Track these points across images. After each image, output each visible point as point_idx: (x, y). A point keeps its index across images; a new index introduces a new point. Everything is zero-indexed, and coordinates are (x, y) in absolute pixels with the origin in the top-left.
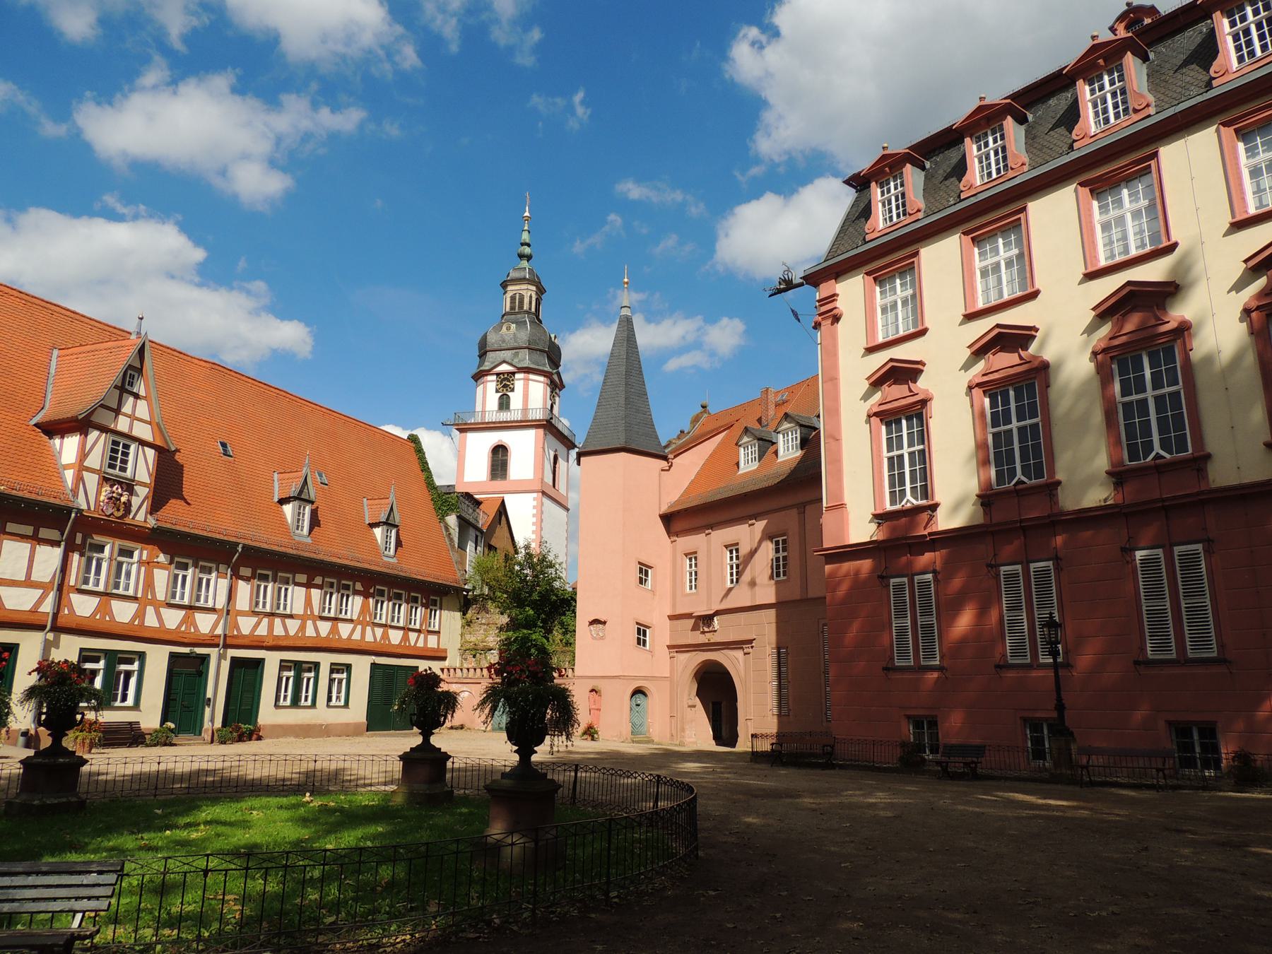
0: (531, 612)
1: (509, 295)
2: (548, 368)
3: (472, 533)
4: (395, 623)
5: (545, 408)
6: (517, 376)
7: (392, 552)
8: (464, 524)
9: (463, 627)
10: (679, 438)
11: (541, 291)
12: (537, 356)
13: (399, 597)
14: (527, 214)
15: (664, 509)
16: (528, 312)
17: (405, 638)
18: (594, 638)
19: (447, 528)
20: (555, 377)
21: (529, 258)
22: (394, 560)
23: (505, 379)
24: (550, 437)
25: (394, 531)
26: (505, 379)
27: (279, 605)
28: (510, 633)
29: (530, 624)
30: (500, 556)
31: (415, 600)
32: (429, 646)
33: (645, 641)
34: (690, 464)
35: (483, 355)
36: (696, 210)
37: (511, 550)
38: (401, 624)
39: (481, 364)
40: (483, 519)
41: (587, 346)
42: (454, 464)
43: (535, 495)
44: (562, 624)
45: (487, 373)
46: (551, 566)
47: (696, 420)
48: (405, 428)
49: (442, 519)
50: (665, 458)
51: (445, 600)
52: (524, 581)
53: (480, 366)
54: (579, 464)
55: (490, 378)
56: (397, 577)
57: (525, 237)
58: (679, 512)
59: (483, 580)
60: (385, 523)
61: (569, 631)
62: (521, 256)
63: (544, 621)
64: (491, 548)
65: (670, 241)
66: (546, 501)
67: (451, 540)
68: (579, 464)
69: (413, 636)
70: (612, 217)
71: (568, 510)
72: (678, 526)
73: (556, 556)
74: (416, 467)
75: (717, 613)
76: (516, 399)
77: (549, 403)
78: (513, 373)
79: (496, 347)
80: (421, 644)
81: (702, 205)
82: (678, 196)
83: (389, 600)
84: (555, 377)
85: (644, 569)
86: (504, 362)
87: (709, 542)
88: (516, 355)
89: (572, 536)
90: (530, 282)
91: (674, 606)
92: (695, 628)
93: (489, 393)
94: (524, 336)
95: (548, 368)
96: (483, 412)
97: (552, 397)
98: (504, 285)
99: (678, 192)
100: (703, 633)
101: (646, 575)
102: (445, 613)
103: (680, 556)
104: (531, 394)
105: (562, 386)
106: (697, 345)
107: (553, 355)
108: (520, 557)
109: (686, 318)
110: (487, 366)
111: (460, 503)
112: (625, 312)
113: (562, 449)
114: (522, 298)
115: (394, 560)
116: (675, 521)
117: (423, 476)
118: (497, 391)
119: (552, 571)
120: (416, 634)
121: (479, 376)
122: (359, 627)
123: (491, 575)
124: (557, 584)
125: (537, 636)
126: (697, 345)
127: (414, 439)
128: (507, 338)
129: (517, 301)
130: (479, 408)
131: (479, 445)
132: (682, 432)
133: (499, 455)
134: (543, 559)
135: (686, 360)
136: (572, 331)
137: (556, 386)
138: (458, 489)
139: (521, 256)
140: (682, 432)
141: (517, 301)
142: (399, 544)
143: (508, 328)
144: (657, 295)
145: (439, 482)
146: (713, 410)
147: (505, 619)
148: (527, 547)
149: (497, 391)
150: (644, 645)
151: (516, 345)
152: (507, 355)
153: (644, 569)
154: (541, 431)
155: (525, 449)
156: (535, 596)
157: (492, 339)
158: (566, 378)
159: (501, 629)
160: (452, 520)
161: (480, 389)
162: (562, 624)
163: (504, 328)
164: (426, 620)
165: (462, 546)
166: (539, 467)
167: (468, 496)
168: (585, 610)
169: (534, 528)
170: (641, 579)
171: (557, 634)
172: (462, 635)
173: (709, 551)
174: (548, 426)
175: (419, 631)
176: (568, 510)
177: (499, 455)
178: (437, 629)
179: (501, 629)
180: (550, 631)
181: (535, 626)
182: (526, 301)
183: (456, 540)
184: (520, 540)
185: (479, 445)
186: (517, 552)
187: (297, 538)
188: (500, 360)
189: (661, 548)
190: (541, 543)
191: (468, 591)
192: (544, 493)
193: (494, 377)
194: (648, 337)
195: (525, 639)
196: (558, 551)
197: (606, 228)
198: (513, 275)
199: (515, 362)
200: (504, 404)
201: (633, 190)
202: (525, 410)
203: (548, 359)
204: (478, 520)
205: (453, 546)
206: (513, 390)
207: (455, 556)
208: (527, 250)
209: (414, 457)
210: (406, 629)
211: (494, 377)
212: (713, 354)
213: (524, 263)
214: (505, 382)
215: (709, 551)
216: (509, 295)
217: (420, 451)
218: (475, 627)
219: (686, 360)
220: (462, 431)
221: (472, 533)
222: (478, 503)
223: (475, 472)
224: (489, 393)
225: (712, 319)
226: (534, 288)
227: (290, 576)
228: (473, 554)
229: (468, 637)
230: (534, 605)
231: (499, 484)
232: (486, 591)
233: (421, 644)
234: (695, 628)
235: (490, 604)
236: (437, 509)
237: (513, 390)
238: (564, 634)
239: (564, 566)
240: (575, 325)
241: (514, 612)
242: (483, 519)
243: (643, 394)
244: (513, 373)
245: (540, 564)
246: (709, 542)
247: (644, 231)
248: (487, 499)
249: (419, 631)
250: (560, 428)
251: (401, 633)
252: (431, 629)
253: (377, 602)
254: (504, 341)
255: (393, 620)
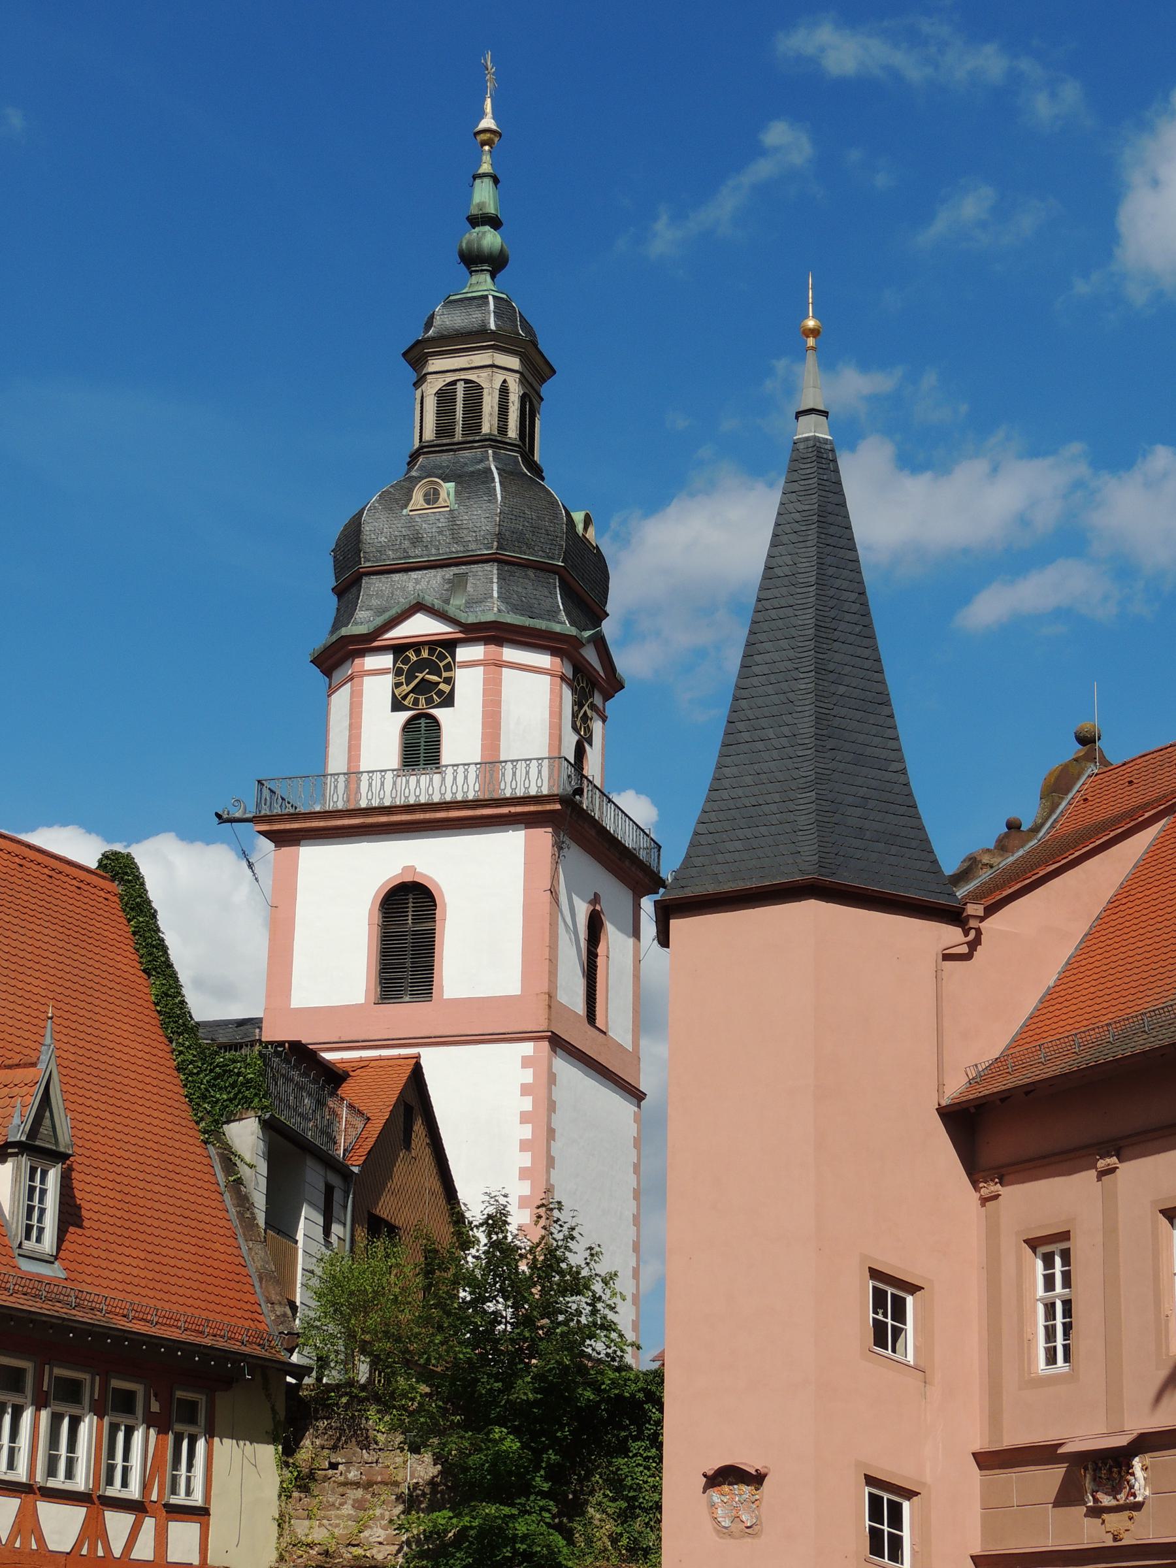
0: (511, 1444)
1: (432, 386)
2: (563, 625)
3: (314, 1177)
4: (59, 1482)
5: (556, 758)
6: (463, 653)
7: (48, 1243)
8: (288, 1148)
9: (284, 1494)
10: (1002, 846)
11: (536, 371)
12: (527, 586)
13: (70, 1392)
14: (488, 123)
15: (955, 1087)
16: (497, 442)
17: (94, 1530)
18: (724, 1532)
19: (229, 1160)
20: (590, 655)
21: (496, 263)
22: (55, 1271)
23: (422, 665)
24: (575, 855)
25: (53, 1176)
26: (422, 665)
27: (52, 1462)
28: (442, 1517)
29: (506, 1485)
30: (409, 1258)
31: (125, 1403)
32: (174, 1556)
33: (896, 1544)
34: (1042, 935)
35: (347, 588)
36: (1054, 103)
37: (444, 1233)
38: (80, 1484)
39: (344, 614)
40: (351, 1133)
41: (695, 555)
42: (257, 944)
43: (528, 1048)
44: (616, 1484)
45: (365, 644)
46: (577, 1285)
47: (1058, 786)
48: (90, 826)
49: (213, 1133)
50: (954, 916)
51: (223, 1401)
52: (485, 1337)
53: (338, 623)
54: (664, 939)
55: (372, 662)
56: (62, 1326)
57: (484, 196)
58: (1005, 1098)
59: (351, 1335)
60: (23, 1148)
61: (641, 1508)
62: (472, 260)
63: (556, 1475)
64: (377, 1226)
65: (972, 205)
66: (567, 1071)
67: (243, 1201)
68: (664, 939)
69: (118, 1524)
70: (778, 134)
71: (637, 1096)
72: (999, 1145)
73: (593, 1254)
74: (127, 961)
75: (1145, 1443)
76: (460, 730)
77: (570, 740)
78: (450, 645)
79: (391, 557)
80: (144, 1550)
81: (1071, 92)
82: (990, 62)
83: (39, 1405)
84: (590, 655)
85: (890, 1296)
86: (419, 607)
87: (1109, 1200)
88: (458, 584)
89: (649, 1192)
90: (501, 341)
91: (995, 1418)
92: (1067, 1496)
93: (367, 719)
94: (482, 519)
95: (563, 625)
96: (353, 774)
97: (581, 724)
98: (417, 356)
99: (989, 49)
100: (1097, 1512)
101: (899, 1313)
102: (225, 1448)
103: (1011, 1247)
104: (508, 712)
105: (613, 684)
106: (1069, 542)
107: (583, 580)
108: (472, 1259)
109: (1034, 452)
110: (362, 622)
111: (277, 1075)
112: (810, 428)
113: (615, 895)
114: (474, 393)
115: (55, 1271)
116: (996, 1130)
117: (148, 989)
118: (397, 705)
119: (577, 1302)
120: (128, 1519)
121: (336, 658)
122: (149, 1523)
123: (375, 1318)
124: (598, 1347)
125: (530, 1523)
126: (1069, 542)
127: (119, 869)
128: (428, 530)
129: (458, 404)
130: (337, 762)
131: (341, 884)
132: (1013, 826)
133: (408, 916)
134: (550, 1261)
135: (1034, 592)
136: (655, 502)
137: (591, 683)
138: (272, 1032)
139: (472, 260)
140: (1013, 826)
141: (458, 404)
142: (70, 1214)
143: (432, 497)
144: (930, 379)
145: (203, 1007)
146: (1115, 749)
147: (421, 1469)
148: (496, 1222)
149: (397, 705)
150: (896, 1556)
151: (456, 549)
152: (429, 584)
153: (890, 1296)
154: (544, 836)
155: (488, 891)
156: (524, 1391)
157: (379, 531)
158: (624, 663)
159: (411, 1502)
160: (245, 1135)
161: (340, 700)
162: (616, 1484)
163: (418, 497)
164: (164, 1469)
165: (281, 1223)
166: (540, 956)
167: (301, 1055)
168: (690, 1440)
169: (526, 1160)
170: (879, 1327)
171: (600, 1519)
172: (282, 1521)
173: (1110, 1230)
174: (568, 818)
175: (138, 1508)
176: (637, 1096)
177: (408, 916)
178: (197, 1499)
179: (411, 1502)
180: (574, 1508)
181: (526, 1489)
182: (490, 404)
183: (259, 1200)
184: (474, 1206)
185: (341, 884)
186: (466, 1243)
187: (26, 1266)
188: (404, 602)
189: (942, 1220)
190: (547, 1208)
191: (300, 1372)
192: (557, 1043)
193: (386, 661)
194: (891, 515)
195: (492, 1537)
196: (604, 1237)
197: (763, 169)
198: (447, 320)
199: (457, 604)
200: (421, 746)
201: (840, 50)
202: (491, 764)
203: (561, 594)
204: (331, 1130)
205: (250, 1224)
206: (448, 701)
207: (255, 1257)
208: (490, 239)
209: (120, 929)
210: (94, 1502)
211: (386, 661)
212: (1123, 569)
213: (483, 284)
214: (424, 679)
215: (1110, 1230)
216: (432, 386)
217: (139, 909)
218: (327, 1493)
219: (1034, 592)
220: (282, 839)
221: (314, 1177)
222: (334, 1077)
223: (328, 975)
224: (367, 719)
225: (1116, 455)
226: (514, 362)
227: (201, 1399)
228: (318, 1248)
229: (301, 1528)
230: (521, 1419)
231: (406, 1016)
232: (363, 1371)
233: (144, 1550)
234: (1067, 1496)
235: (374, 1421)
236: (197, 1098)
237: (448, 701)
238: (625, 1517)
239: (624, 1284)
240: (661, 487)
241: (455, 1445)
242: (351, 1133)
243: (878, 702)
244: (450, 645)
245: (548, 1278)
246: (1109, 1200)
247: (882, 180)
248: (364, 1064)
249: (138, 1508)
250: (609, 823)
251: (78, 1514)
252: (180, 1499)
253: (56, 1420)
254: (416, 540)
255: (52, 1471)
